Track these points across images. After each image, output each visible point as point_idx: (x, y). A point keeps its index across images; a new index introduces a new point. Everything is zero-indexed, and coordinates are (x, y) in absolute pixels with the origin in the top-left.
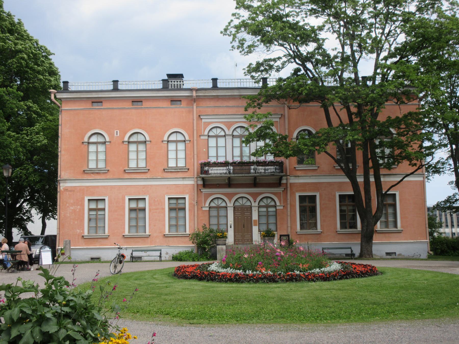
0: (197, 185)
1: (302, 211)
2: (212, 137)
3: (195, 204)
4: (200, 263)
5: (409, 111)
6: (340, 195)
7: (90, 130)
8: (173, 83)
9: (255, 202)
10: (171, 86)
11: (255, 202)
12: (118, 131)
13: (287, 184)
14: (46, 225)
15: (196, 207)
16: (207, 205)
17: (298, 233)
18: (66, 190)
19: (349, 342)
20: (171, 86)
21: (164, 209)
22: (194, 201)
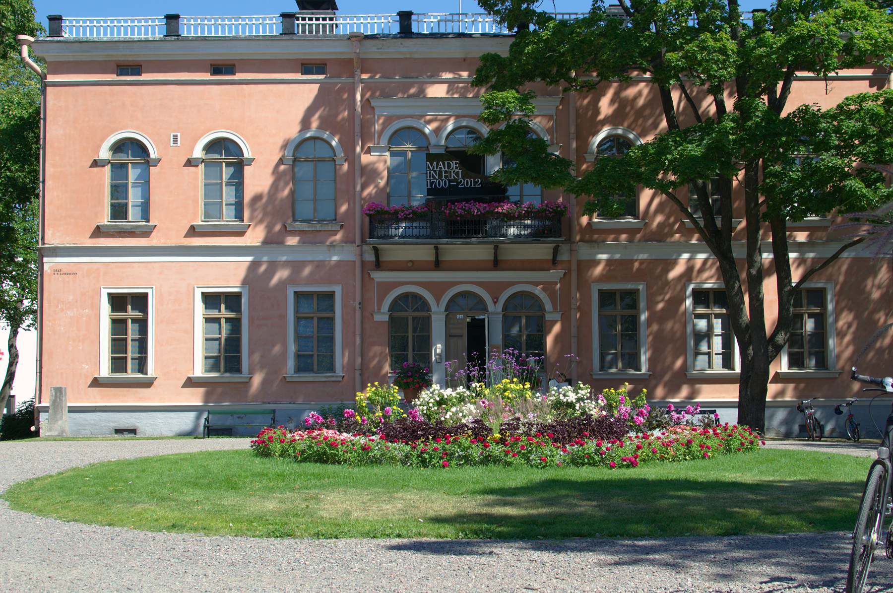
0: (363, 263)
1: (607, 324)
2: (307, 160)
3: (357, 306)
4: (737, 509)
5: (280, 142)
6: (331, 295)
7: (113, 131)
8: (307, 21)
9: (495, 303)
10: (304, 31)
11: (495, 303)
12: (179, 134)
13: (569, 262)
14: (17, 356)
15: (358, 314)
16: (386, 306)
17: (595, 377)
18: (57, 271)
19: (616, 589)
20: (304, 31)
21: (284, 317)
22: (354, 301)
